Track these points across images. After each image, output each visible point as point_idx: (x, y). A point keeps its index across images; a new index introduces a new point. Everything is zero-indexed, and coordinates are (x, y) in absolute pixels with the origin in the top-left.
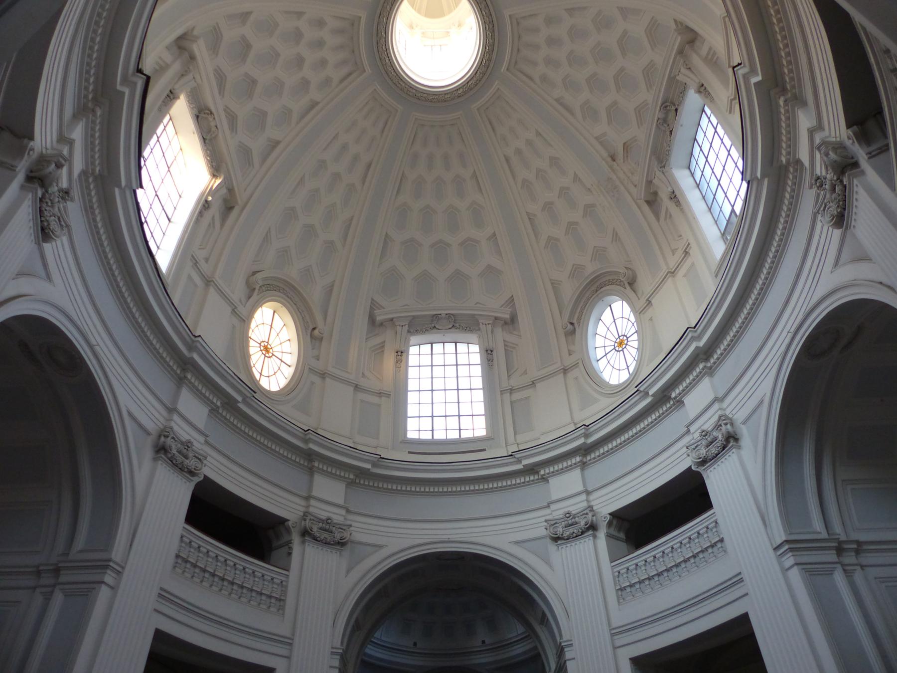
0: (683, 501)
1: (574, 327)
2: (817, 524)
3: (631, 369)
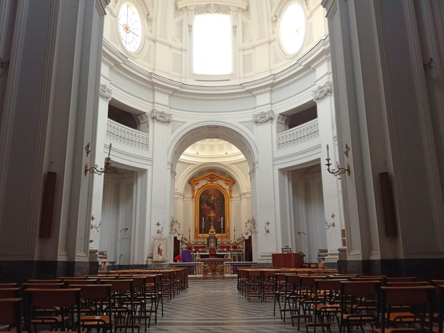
0: (307, 113)
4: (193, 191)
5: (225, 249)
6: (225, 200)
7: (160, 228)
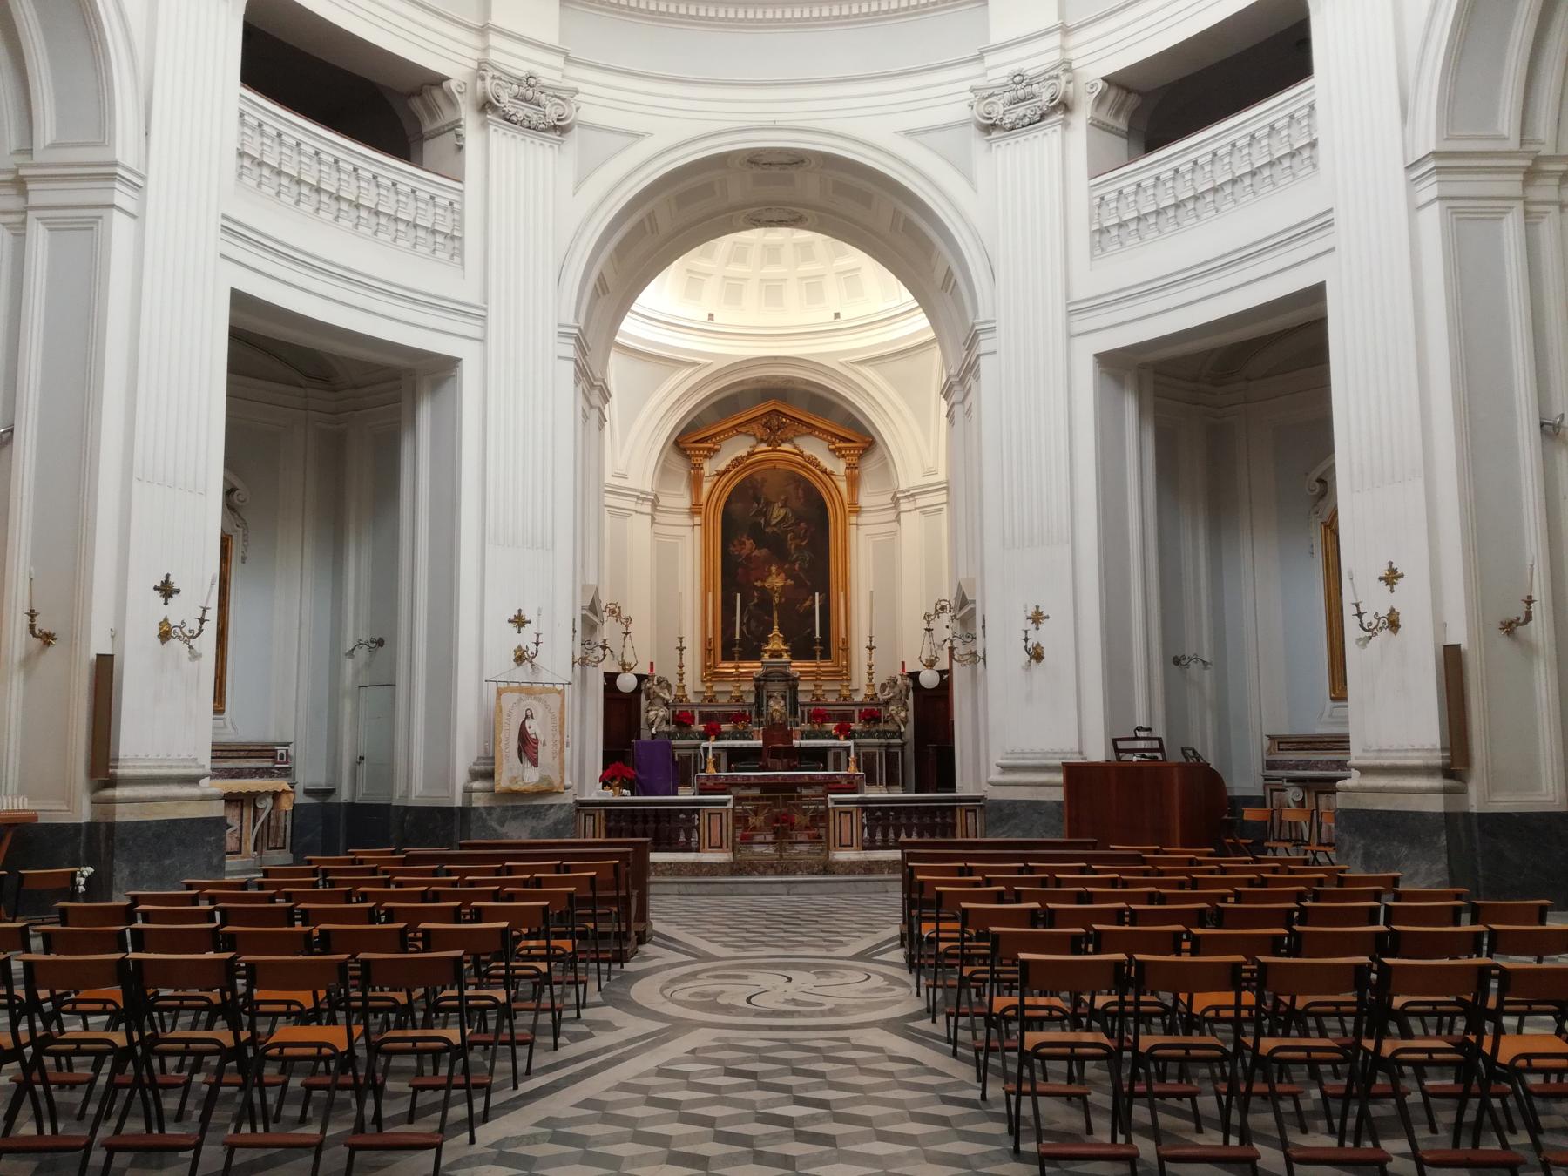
2: (1507, 123)
4: (695, 482)
5: (831, 726)
6: (832, 520)
7: (526, 638)
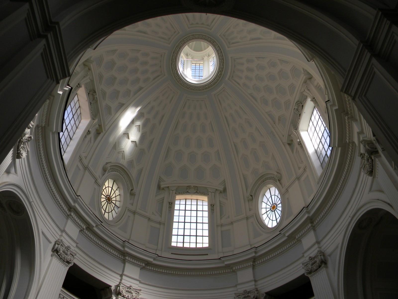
1: (253, 198)
3: (278, 220)
